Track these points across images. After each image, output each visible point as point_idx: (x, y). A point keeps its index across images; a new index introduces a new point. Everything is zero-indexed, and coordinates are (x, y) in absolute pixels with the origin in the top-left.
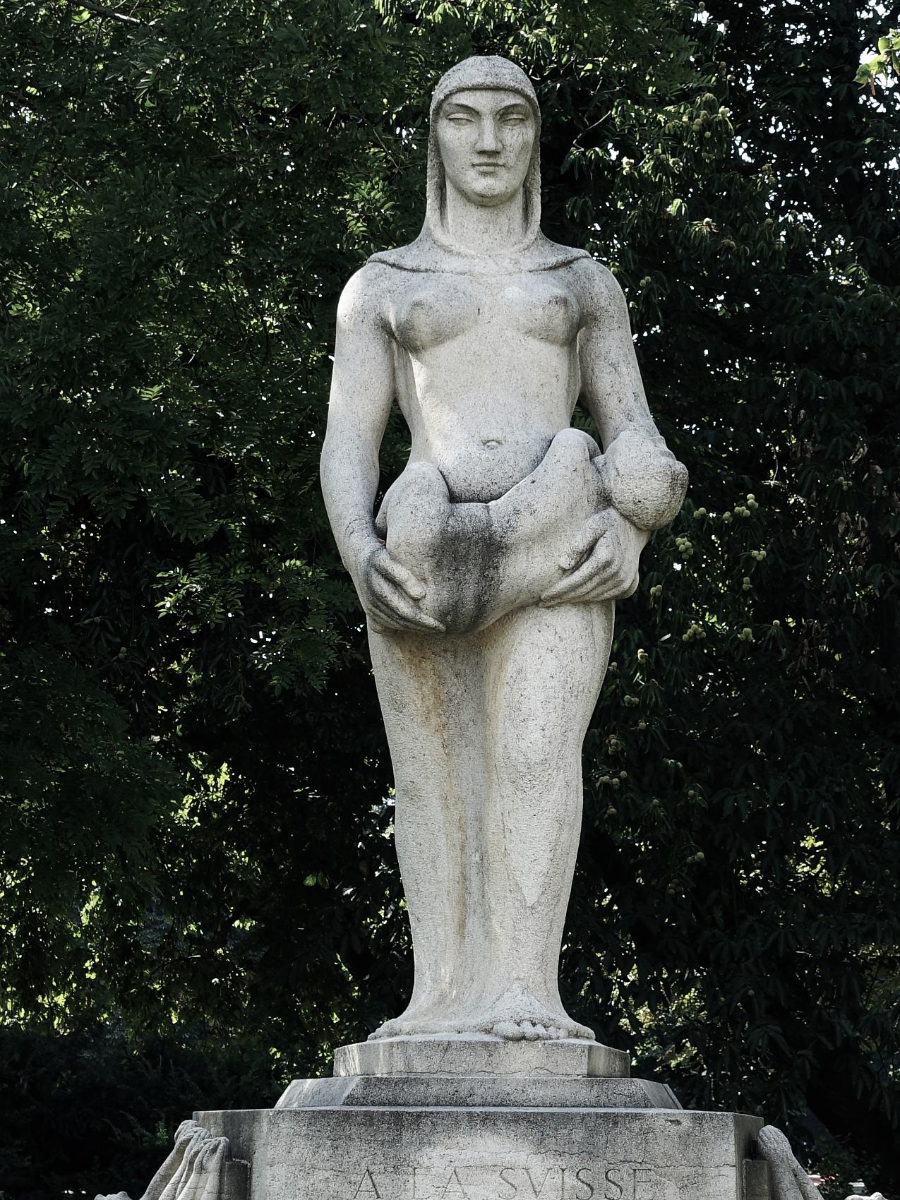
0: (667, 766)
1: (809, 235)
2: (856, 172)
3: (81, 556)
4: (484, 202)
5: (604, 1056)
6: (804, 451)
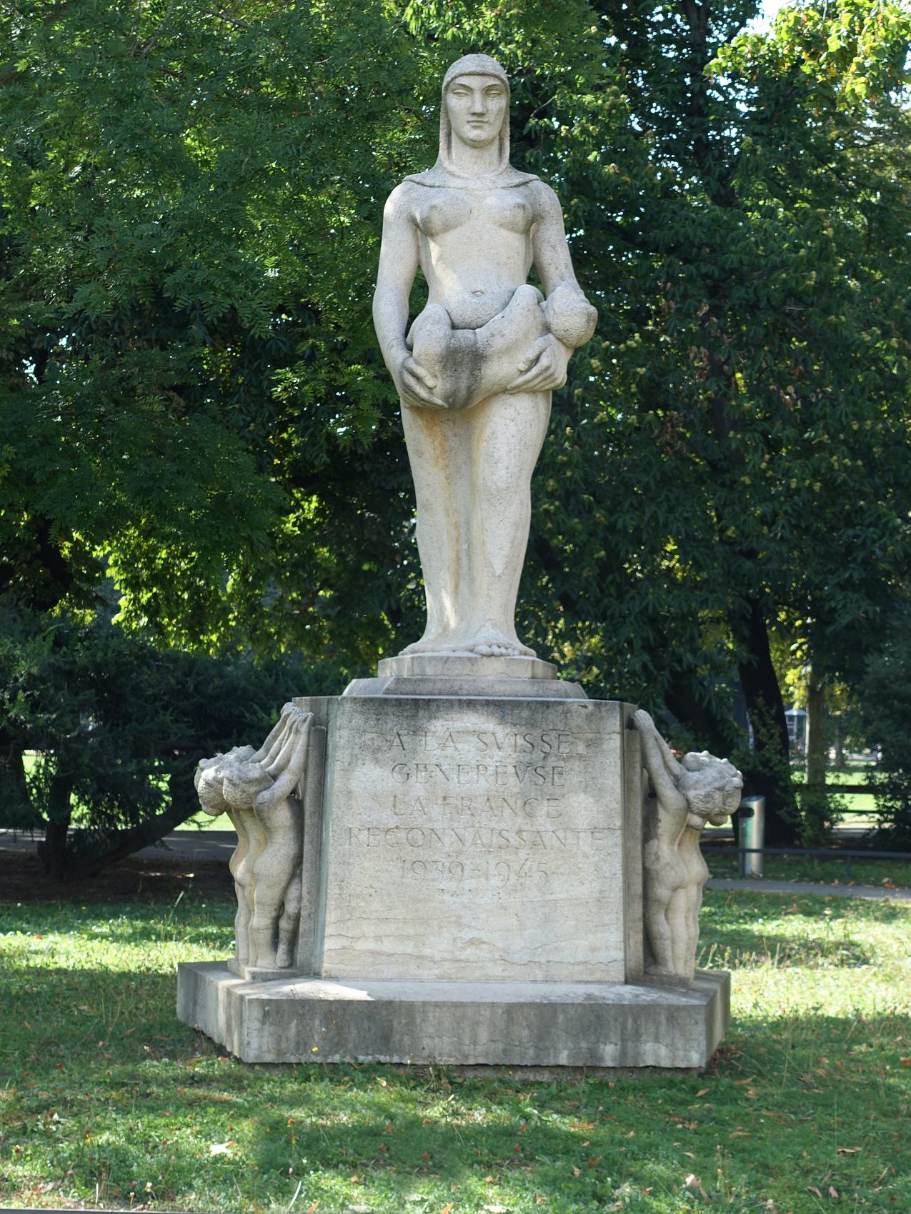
0: (583, 500)
1: (675, 174)
2: (704, 137)
3: (228, 367)
4: (475, 145)
5: (541, 667)
6: (670, 308)
